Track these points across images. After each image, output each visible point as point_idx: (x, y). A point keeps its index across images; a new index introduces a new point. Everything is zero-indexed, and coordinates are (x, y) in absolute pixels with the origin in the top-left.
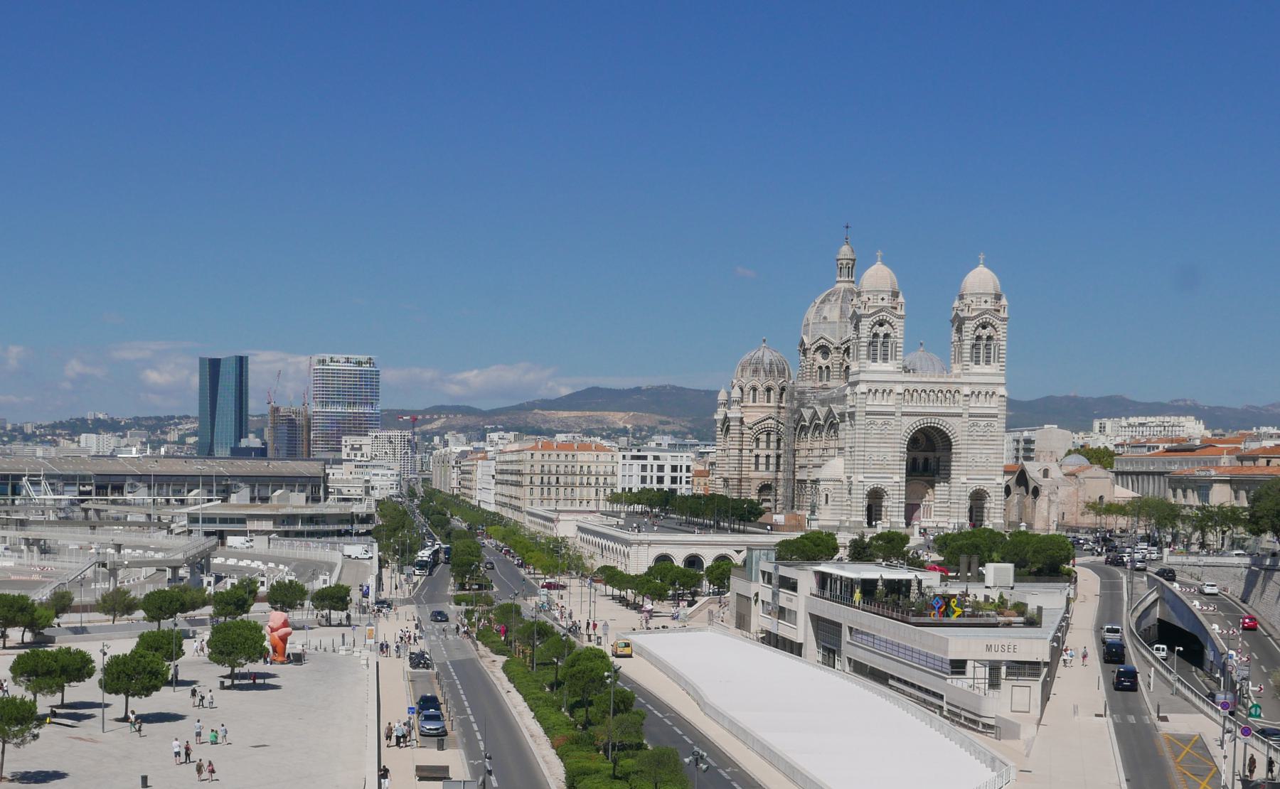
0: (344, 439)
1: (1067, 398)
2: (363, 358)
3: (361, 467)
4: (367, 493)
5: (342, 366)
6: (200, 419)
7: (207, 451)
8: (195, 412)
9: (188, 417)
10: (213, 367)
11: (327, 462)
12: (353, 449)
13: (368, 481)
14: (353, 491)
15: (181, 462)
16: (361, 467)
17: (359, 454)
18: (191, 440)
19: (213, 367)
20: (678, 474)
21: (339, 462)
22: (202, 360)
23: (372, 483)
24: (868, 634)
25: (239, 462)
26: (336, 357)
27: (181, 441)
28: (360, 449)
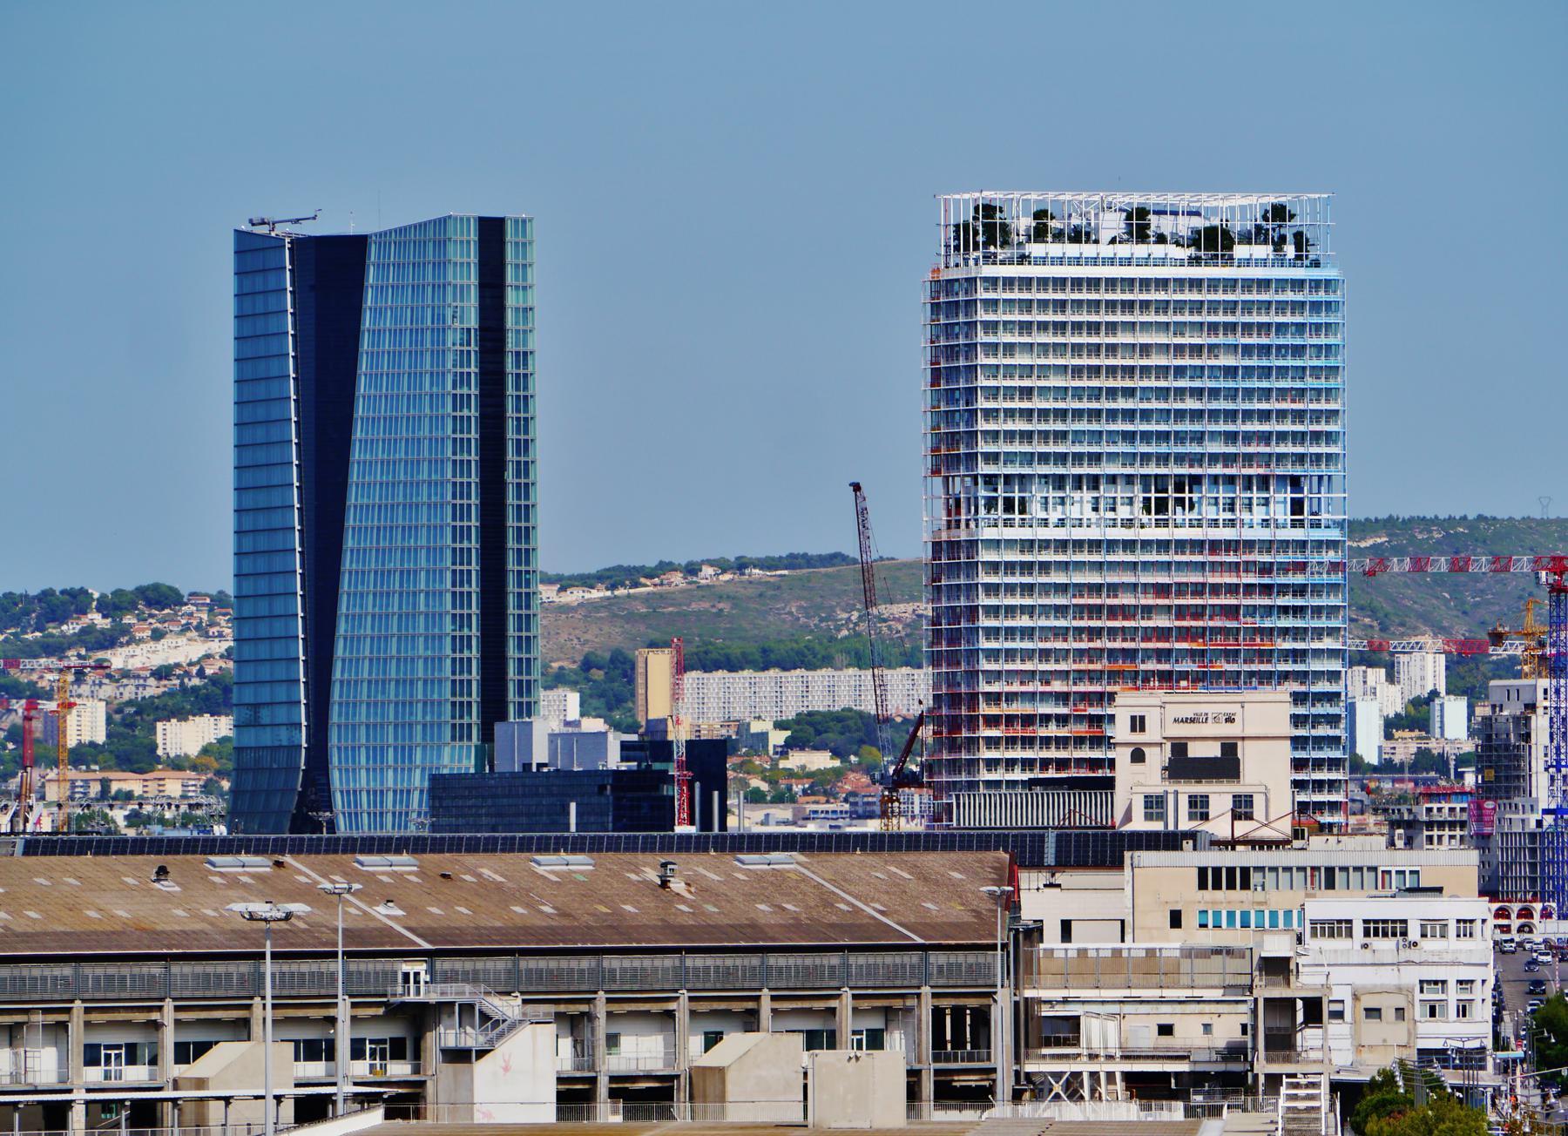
0: (1127, 702)
1: (170, 588)
2: (1238, 206)
3: (1240, 878)
4: (1281, 1043)
5: (1110, 256)
6: (250, 607)
7: (282, 803)
8: (208, 562)
9: (160, 598)
10: (318, 292)
11: (1025, 851)
12: (1182, 765)
13: (1278, 967)
14: (1189, 1033)
15: (133, 871)
16: (1240, 878)
17: (1220, 796)
18: (186, 737)
19: (318, 292)
20: (1229, 516)
21: (1101, 850)
22: (252, 251)
23: (1306, 983)
24: (951, 371)
25: (490, 868)
26: (1071, 203)
27: (130, 743)
28: (1226, 765)
